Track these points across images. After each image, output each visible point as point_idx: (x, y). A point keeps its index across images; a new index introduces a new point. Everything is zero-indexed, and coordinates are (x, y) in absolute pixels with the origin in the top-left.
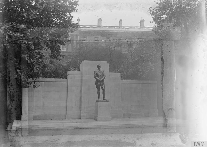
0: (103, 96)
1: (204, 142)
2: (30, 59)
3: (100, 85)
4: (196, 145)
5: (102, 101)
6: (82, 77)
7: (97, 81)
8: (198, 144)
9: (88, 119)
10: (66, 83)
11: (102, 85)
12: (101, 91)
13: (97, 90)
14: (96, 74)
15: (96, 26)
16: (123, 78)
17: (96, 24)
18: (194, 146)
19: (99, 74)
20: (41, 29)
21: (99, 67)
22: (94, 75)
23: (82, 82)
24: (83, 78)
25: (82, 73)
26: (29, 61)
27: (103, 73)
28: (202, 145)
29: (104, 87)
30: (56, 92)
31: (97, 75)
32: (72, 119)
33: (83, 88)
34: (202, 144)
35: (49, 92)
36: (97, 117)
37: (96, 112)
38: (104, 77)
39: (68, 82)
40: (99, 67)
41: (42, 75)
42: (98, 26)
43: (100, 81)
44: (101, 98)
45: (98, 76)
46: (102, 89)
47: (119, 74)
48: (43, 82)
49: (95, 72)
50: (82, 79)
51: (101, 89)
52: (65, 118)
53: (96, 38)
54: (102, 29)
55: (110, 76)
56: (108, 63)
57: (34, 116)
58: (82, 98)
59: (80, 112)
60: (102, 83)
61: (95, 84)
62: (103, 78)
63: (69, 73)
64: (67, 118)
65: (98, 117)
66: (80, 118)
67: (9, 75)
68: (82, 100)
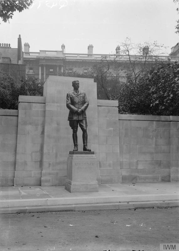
0: (84, 143)
3: (77, 121)
5: (81, 153)
6: (45, 107)
9: (56, 186)
11: (82, 121)
12: (80, 132)
14: (69, 99)
15: (85, 54)
16: (122, 111)
17: (86, 51)
19: (77, 100)
21: (76, 86)
22: (67, 101)
23: (44, 116)
24: (47, 109)
25: (45, 100)
27: (84, 97)
29: (86, 126)
32: (25, 186)
33: (46, 128)
36: (70, 184)
37: (69, 175)
38: (85, 105)
39: (18, 116)
40: (76, 86)
42: (88, 55)
43: (77, 113)
44: (80, 148)
45: (73, 103)
46: (82, 129)
49: (68, 95)
50: (45, 111)
51: (79, 128)
52: (12, 184)
53: (85, 70)
54: (93, 58)
55: (100, 107)
59: (41, 173)
60: (81, 118)
62: (83, 108)
63: (21, 98)
65: (72, 184)
66: (41, 185)
67: (30, 124)
68: (45, 151)
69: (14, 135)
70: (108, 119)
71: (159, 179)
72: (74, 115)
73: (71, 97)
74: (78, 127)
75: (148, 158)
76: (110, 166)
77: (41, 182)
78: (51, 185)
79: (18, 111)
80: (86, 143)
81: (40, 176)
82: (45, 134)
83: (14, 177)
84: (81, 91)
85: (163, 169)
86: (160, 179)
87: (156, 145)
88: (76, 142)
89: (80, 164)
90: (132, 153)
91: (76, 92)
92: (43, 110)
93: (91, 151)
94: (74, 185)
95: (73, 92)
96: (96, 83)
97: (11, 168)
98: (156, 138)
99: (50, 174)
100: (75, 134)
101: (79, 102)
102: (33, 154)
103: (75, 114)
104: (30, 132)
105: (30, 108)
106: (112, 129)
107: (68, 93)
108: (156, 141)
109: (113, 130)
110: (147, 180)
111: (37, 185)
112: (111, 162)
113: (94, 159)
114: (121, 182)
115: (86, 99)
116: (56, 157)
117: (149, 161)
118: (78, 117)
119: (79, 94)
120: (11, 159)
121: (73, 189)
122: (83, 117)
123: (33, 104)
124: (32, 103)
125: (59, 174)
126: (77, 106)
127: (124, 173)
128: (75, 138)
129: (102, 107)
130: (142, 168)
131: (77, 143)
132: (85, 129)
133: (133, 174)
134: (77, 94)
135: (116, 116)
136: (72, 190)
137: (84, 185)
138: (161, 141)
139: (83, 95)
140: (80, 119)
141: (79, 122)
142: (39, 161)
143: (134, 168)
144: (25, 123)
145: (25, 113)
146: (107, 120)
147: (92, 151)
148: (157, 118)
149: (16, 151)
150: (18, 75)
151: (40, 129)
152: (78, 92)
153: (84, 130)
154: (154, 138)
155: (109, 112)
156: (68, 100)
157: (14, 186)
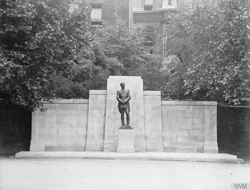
1: (246, 184)
2: (30, 85)
3: (122, 108)
4: (237, 188)
6: (106, 97)
7: (120, 103)
8: (239, 186)
10: (87, 105)
11: (126, 108)
13: (121, 114)
18: (235, 189)
19: (123, 95)
20: (41, 57)
21: (123, 86)
26: (29, 87)
28: (245, 188)
29: (129, 111)
30: (73, 116)
31: (119, 96)
34: (245, 186)
35: (65, 116)
38: (128, 98)
39: (88, 104)
40: (123, 86)
41: (55, 95)
45: (120, 97)
47: (159, 93)
48: (58, 104)
50: (106, 100)
51: (125, 113)
56: (142, 79)
57: (45, 147)
58: (106, 125)
60: (125, 106)
61: (117, 107)
62: (126, 100)
65: (118, 147)
67: (97, 109)
68: (106, 128)
69: (86, 117)
70: (153, 104)
71: (194, 150)
75: (186, 133)
76: (154, 138)
79: (89, 101)
81: (103, 145)
82: (106, 116)
85: (199, 143)
86: (196, 150)
87: (193, 124)
88: (123, 121)
92: (105, 99)
93: (130, 127)
95: (121, 90)
96: (142, 80)
97: (84, 139)
98: (192, 119)
99: (109, 143)
104: (97, 114)
106: (156, 112)
108: (192, 121)
110: (184, 151)
112: (155, 136)
113: (132, 132)
114: (163, 151)
116: (114, 131)
117: (187, 136)
120: (84, 133)
121: (119, 150)
126: (123, 99)
127: (166, 145)
128: (122, 119)
129: (148, 96)
130: (180, 141)
136: (118, 151)
137: (126, 148)
138: (197, 121)
141: (124, 109)
143: (175, 141)
144: (93, 109)
145: (93, 102)
147: (131, 127)
148: (194, 103)
150: (117, 5)
151: (103, 112)
154: (191, 118)
155: (154, 99)
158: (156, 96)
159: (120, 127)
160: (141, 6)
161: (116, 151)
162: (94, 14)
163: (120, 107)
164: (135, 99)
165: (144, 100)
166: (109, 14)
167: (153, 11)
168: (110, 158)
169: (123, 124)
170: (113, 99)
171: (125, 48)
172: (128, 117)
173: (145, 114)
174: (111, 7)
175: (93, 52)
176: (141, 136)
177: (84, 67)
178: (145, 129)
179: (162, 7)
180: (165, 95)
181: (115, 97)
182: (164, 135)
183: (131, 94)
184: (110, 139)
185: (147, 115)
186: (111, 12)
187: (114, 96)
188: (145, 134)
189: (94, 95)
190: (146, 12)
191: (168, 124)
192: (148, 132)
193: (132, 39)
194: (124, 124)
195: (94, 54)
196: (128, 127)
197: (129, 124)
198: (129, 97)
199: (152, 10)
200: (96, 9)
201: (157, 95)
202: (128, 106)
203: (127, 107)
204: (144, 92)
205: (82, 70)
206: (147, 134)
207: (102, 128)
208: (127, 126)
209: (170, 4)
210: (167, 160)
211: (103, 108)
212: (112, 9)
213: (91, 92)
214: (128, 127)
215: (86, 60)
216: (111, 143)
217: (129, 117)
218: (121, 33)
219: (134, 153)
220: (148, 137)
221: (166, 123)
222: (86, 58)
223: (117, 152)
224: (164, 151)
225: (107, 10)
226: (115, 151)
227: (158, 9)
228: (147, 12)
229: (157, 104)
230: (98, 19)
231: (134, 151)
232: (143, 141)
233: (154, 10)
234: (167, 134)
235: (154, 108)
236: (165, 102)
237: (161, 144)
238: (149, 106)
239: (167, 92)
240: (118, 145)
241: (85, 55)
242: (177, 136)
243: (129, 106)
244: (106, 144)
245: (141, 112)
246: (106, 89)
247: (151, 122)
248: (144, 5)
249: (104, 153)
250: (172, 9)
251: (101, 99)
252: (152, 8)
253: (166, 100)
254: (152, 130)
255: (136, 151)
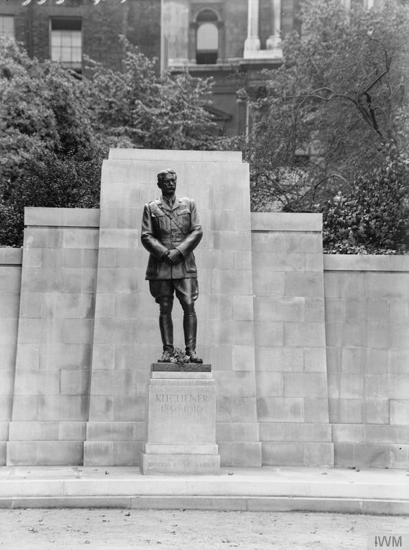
1: (400, 538)
3: (167, 280)
4: (381, 545)
6: (97, 238)
7: (157, 260)
8: (385, 541)
10: (14, 270)
11: (181, 281)
13: (158, 306)
14: (149, 222)
19: (168, 224)
21: (166, 185)
22: (143, 229)
25: (98, 219)
28: (397, 546)
29: (194, 294)
38: (190, 239)
39: (21, 265)
40: (166, 185)
45: (158, 233)
49: (145, 208)
50: (97, 251)
51: (176, 301)
58: (95, 354)
60: (177, 273)
62: (182, 246)
64: (8, 463)
65: (148, 450)
67: (56, 287)
68: (96, 364)
70: (288, 269)
72: (161, 266)
73: (153, 216)
74: (173, 297)
76: (295, 410)
77: (82, 451)
78: (112, 464)
80: (191, 341)
82: (97, 315)
83: (8, 440)
84: (181, 200)
88: (167, 338)
89: (169, 397)
90: (370, 376)
91: (168, 203)
92: (92, 246)
93: (201, 362)
94: (151, 454)
95: (159, 202)
99: (108, 431)
100: (165, 316)
101: (172, 230)
102: (64, 372)
103: (164, 264)
105: (57, 242)
106: (303, 299)
107: (147, 205)
109: (306, 302)
111: (73, 464)
112: (300, 400)
113: (209, 383)
114: (332, 463)
115: (195, 219)
116: (128, 381)
118: (169, 270)
119: (174, 207)
121: (150, 465)
122: (183, 272)
123: (64, 230)
124: (62, 227)
125: (134, 431)
126: (168, 241)
127: (345, 436)
128: (165, 327)
129: (270, 235)
131: (171, 341)
132: (189, 302)
133: (376, 441)
134: (169, 208)
135: (314, 258)
136: (145, 467)
137: (180, 454)
139: (188, 210)
140: (174, 277)
142: (82, 395)
144: (41, 286)
145: (42, 258)
146: (286, 272)
149: (14, 364)
150: (125, 22)
152: (173, 202)
153: (187, 305)
155: (292, 248)
156: (146, 224)
157: (5, 465)
158: (303, 235)
159: (155, 362)
160: (186, 52)
161: (134, 462)
162: (61, 47)
163: (156, 274)
164: (216, 246)
165: (256, 251)
166: (104, 48)
167: (221, 67)
168: (113, 503)
169: (168, 348)
170: (127, 248)
171: (150, 136)
172: (192, 321)
173: (256, 309)
174: (110, 29)
175: (50, 112)
176: (242, 399)
177: (17, 159)
178: (258, 372)
179: (242, 56)
180: (332, 236)
181: (133, 236)
182: (335, 396)
183: (203, 220)
184: (111, 413)
185: (266, 314)
186: (109, 42)
187: (127, 231)
188: (258, 389)
189: (46, 230)
190: (200, 69)
191: (353, 350)
192: (269, 382)
193: (172, 110)
194: (172, 347)
195: (53, 122)
196: (192, 360)
197: (194, 347)
198: (196, 233)
199: (217, 65)
200: (67, 33)
201: (306, 232)
202: (191, 272)
203: (188, 275)
204: (252, 219)
205: (12, 168)
206: (264, 394)
207: (77, 368)
208: (188, 357)
209: (263, 47)
210: (371, 509)
211: (84, 283)
212: (111, 32)
213: (32, 214)
214: (192, 360)
215: (26, 137)
216: (114, 431)
217: (195, 316)
218: (138, 92)
219: (216, 474)
220: (268, 401)
221: (343, 345)
222: (25, 130)
223: (142, 472)
224: (336, 466)
225: (96, 35)
226: (135, 465)
227: (232, 60)
228: (203, 69)
229: (308, 269)
230: (71, 62)
231: (217, 466)
232: (252, 424)
233: (221, 65)
234: (348, 393)
235: (293, 284)
236: (341, 261)
237: (323, 434)
238: (270, 274)
239: (341, 225)
240: (146, 440)
241: (21, 121)
242: (389, 400)
243: (196, 272)
244: (97, 433)
245: (243, 300)
246: (98, 207)
247: (281, 344)
248: (197, 50)
249: (84, 480)
250: (271, 60)
251: (74, 245)
252: (217, 58)
253: (341, 253)
254: (285, 376)
255: (228, 465)
